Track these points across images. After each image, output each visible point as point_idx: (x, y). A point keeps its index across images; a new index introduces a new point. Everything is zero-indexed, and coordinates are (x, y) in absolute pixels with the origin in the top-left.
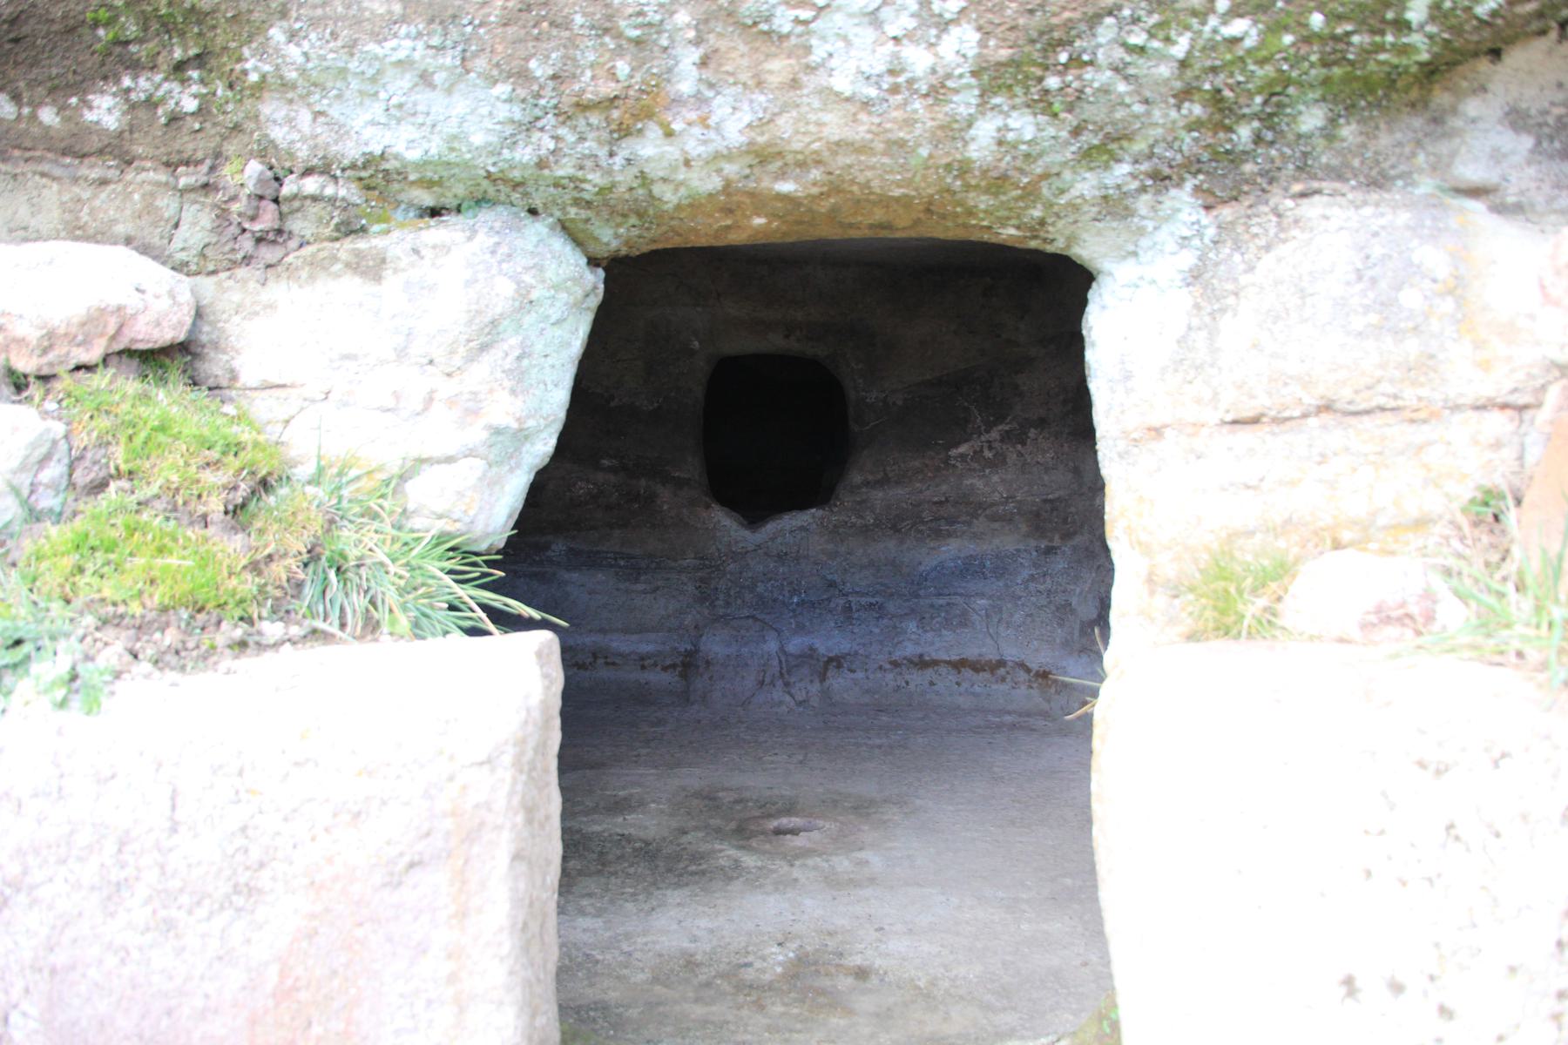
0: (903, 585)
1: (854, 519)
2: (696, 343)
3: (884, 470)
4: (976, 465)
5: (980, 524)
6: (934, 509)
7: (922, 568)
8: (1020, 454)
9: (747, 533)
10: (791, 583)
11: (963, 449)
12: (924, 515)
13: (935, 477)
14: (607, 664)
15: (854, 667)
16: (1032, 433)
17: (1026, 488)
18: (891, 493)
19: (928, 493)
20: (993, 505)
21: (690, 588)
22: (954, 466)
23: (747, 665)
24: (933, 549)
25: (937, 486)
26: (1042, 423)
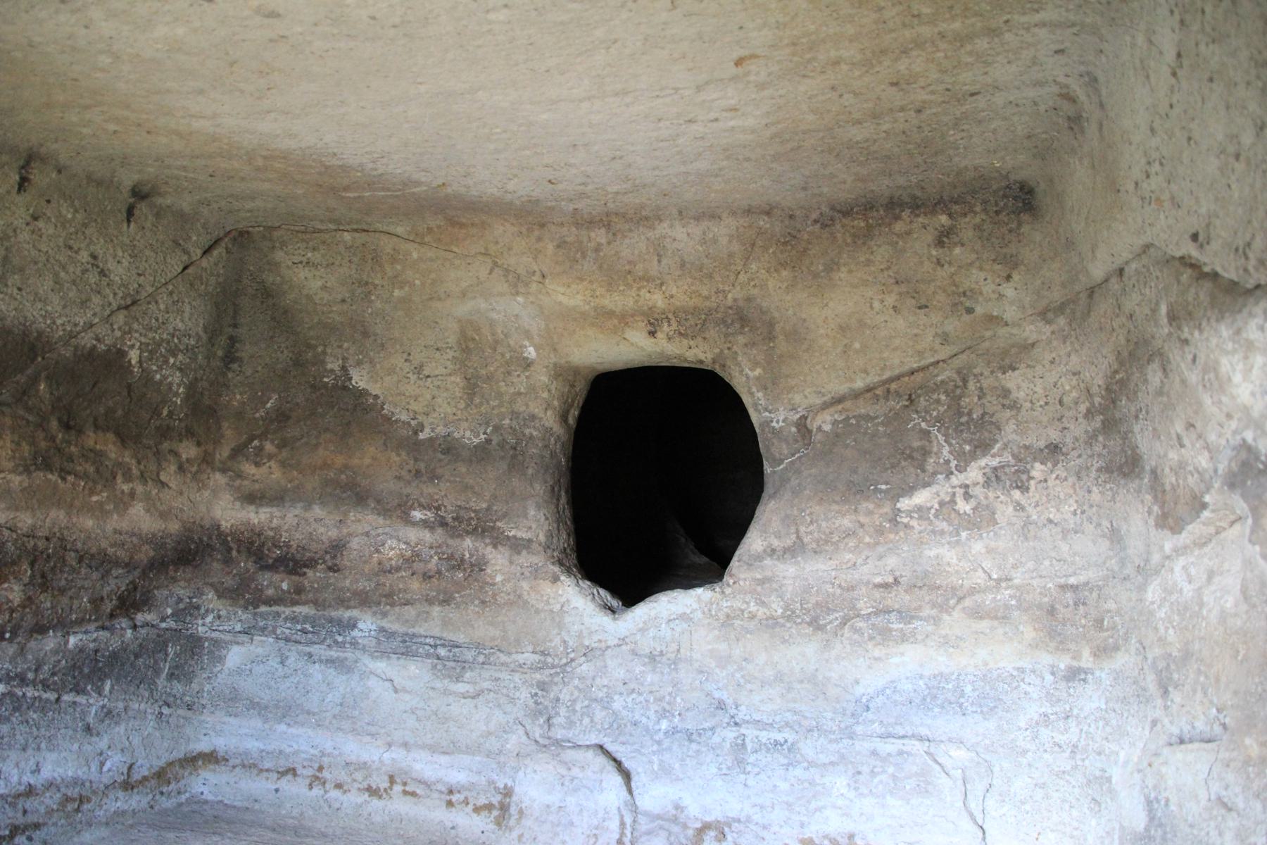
0: (829, 715)
1: (753, 607)
2: (531, 349)
3: (797, 532)
4: (944, 525)
5: (955, 622)
6: (877, 594)
7: (859, 690)
8: (1019, 507)
9: (605, 620)
10: (661, 699)
11: (922, 497)
12: (860, 605)
13: (877, 544)
14: (405, 793)
16: (1038, 470)
17: (1031, 565)
18: (808, 568)
19: (865, 569)
20: (973, 591)
21: (524, 695)
22: (907, 526)
23: (572, 824)
24: (877, 659)
25: (880, 558)
26: (1054, 451)
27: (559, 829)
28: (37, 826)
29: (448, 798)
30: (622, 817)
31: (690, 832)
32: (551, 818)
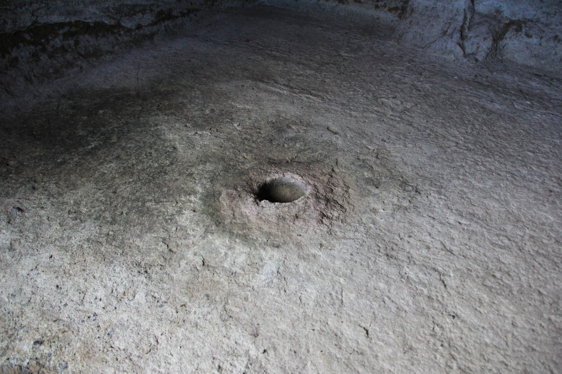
15: (531, 32)
23: (438, 16)
27: (431, 19)
28: (197, 10)
29: (376, 3)
30: (465, 14)
31: (502, 25)
32: (427, 13)
